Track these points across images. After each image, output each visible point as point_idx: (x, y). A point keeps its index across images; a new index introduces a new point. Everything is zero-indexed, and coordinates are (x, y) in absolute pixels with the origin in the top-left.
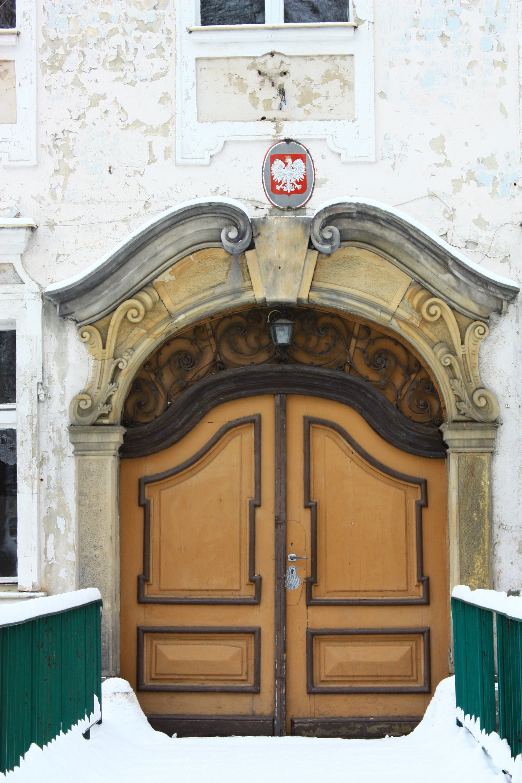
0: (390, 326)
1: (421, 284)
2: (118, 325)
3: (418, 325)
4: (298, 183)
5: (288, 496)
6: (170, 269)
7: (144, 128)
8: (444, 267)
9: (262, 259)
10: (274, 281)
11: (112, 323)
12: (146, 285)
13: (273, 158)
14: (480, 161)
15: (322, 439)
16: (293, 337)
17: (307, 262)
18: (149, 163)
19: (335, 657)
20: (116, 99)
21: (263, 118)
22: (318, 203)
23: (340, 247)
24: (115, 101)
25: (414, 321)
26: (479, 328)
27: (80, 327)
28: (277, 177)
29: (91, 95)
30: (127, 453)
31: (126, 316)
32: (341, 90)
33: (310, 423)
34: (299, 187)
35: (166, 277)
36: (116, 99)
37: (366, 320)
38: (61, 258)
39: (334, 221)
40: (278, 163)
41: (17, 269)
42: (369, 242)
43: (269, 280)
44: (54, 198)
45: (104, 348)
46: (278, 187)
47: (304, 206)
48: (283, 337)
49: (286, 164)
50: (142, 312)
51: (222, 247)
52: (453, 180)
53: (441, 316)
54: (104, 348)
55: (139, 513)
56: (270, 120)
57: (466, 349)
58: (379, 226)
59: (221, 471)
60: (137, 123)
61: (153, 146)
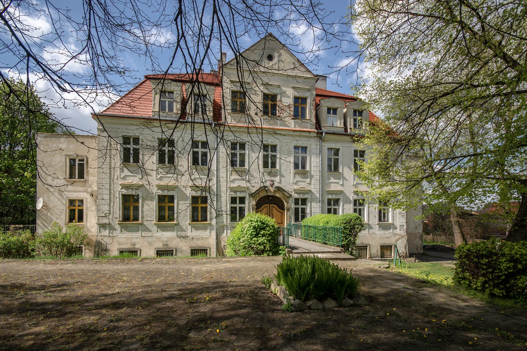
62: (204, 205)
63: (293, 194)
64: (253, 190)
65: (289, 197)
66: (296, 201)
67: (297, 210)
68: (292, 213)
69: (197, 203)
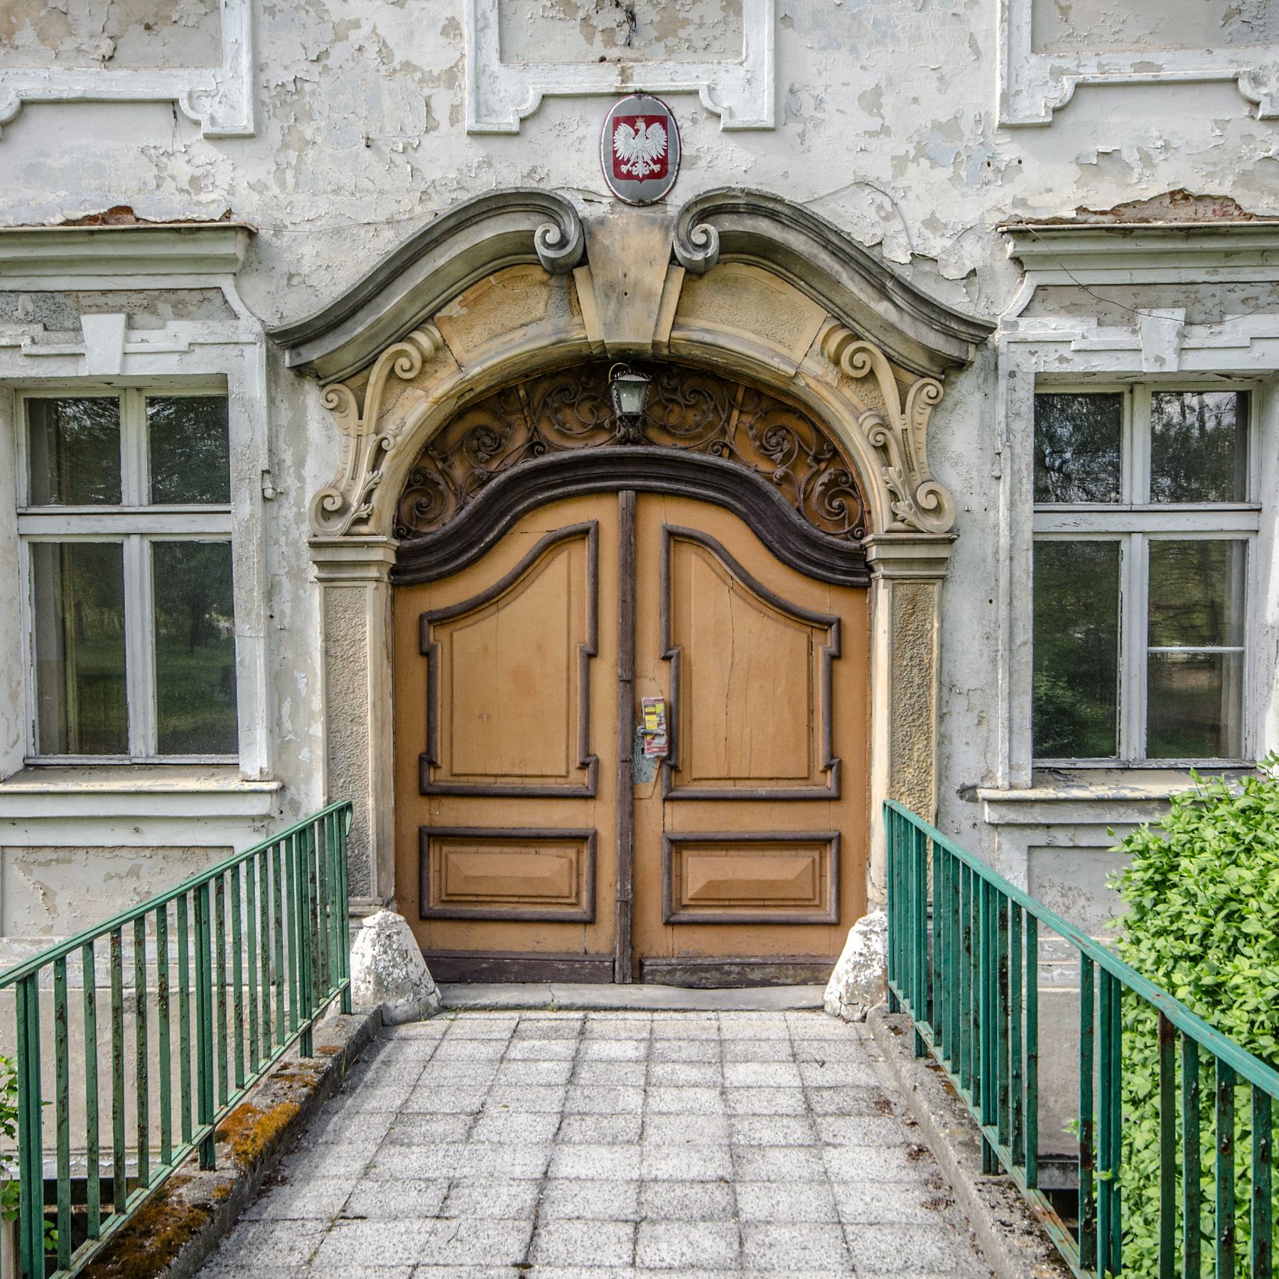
0: (792, 389)
1: (841, 318)
2: (381, 383)
3: (835, 384)
4: (655, 162)
5: (634, 634)
6: (460, 298)
7: (418, 75)
8: (880, 291)
9: (599, 281)
10: (617, 315)
11: (372, 379)
12: (424, 321)
13: (617, 122)
14: (937, 126)
15: (693, 564)
16: (647, 406)
17: (669, 285)
18: (427, 131)
19: (700, 871)
20: (375, 28)
21: (603, 59)
22: (684, 191)
23: (718, 263)
24: (374, 31)
25: (829, 378)
26: (929, 388)
27: (324, 386)
28: (623, 153)
29: (337, 21)
30: (406, 575)
31: (392, 370)
32: (723, 14)
33: (674, 537)
34: (657, 168)
35: (454, 309)
36: (375, 28)
37: (755, 380)
38: (295, 281)
39: (711, 219)
40: (624, 129)
41: (228, 298)
42: (763, 252)
43: (610, 313)
44: (283, 185)
45: (360, 418)
46: (624, 169)
47: (663, 199)
48: (630, 403)
49: (637, 131)
50: (418, 364)
51: (538, 263)
52: (893, 158)
53: (872, 372)
54: (360, 418)
55: (419, 666)
56: (610, 61)
57: (908, 420)
58: (780, 226)
59: (538, 619)
60: (408, 66)
61: (433, 103)
62: (187, 523)
63: (1006, 300)
64: (325, 267)
65: (951, 368)
66: (1076, 429)
67: (1071, 583)
68: (986, 636)
69: (1103, 483)
